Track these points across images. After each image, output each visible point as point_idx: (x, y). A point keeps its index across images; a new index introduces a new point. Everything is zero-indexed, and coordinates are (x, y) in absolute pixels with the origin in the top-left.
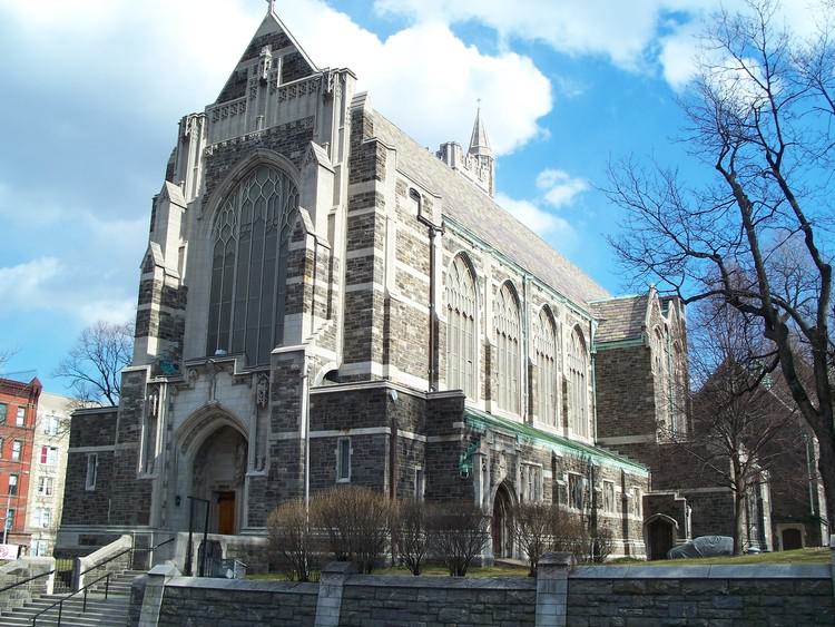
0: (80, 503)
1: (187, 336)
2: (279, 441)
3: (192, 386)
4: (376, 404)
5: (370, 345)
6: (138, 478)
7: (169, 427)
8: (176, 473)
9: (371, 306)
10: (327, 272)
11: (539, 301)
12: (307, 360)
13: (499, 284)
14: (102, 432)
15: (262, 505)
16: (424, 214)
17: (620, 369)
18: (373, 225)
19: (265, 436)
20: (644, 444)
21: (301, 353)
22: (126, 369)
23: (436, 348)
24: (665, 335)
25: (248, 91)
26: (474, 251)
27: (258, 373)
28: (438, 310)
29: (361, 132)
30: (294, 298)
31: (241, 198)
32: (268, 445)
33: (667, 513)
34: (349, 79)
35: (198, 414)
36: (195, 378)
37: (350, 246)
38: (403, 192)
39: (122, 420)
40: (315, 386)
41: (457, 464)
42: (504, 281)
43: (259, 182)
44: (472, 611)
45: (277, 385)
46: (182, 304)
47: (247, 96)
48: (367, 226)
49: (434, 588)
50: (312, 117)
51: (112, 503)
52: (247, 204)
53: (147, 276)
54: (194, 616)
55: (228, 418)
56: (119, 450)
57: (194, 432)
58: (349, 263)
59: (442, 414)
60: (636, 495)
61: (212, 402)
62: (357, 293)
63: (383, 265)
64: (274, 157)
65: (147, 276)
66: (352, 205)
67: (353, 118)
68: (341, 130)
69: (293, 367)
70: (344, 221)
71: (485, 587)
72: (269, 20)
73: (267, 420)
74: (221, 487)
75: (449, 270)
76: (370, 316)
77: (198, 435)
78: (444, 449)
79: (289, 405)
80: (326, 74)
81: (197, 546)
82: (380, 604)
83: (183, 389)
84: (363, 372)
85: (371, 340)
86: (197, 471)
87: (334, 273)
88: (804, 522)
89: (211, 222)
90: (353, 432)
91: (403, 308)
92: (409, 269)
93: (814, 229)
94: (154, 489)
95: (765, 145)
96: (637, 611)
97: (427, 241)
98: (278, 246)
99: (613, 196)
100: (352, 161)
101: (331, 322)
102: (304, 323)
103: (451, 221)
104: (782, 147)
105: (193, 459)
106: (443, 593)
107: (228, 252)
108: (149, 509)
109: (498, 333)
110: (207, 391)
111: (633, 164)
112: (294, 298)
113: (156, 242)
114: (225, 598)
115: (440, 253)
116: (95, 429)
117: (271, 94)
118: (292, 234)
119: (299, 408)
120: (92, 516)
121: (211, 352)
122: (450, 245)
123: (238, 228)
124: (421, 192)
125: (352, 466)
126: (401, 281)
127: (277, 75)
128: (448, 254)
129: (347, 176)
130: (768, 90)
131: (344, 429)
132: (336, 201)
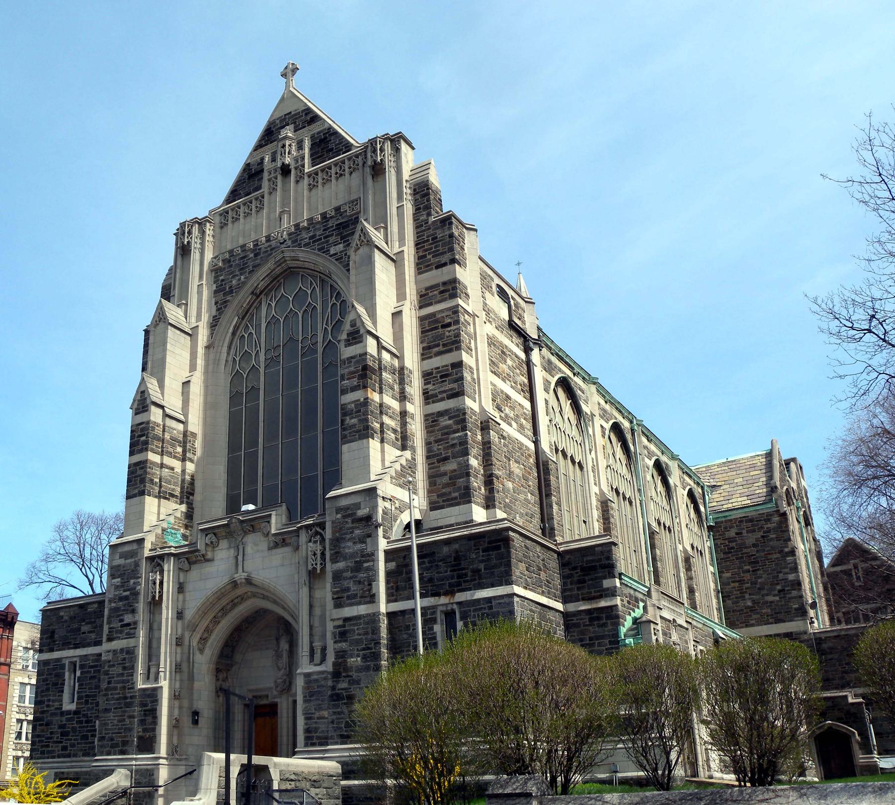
0: (55, 729)
2: (346, 620)
4: (493, 554)
5: (468, 481)
7: (180, 615)
8: (191, 678)
9: (464, 428)
10: (396, 387)
11: (650, 455)
12: (381, 504)
13: (607, 426)
14: (85, 628)
15: (325, 713)
18: (457, 322)
19: (323, 617)
21: (372, 492)
22: (114, 541)
23: (549, 495)
24: (795, 501)
25: (265, 185)
27: (308, 527)
28: (545, 446)
29: (428, 207)
30: (354, 421)
32: (330, 626)
34: (404, 147)
35: (220, 594)
36: (213, 545)
37: (426, 353)
38: (488, 288)
39: (111, 610)
40: (393, 538)
43: (288, 292)
45: (337, 541)
48: (449, 325)
51: (101, 725)
52: (272, 322)
53: (141, 418)
55: (265, 597)
57: (216, 621)
58: (427, 376)
59: (583, 569)
61: (240, 576)
62: (441, 414)
63: (475, 376)
64: (307, 256)
65: (141, 418)
66: (424, 300)
67: (415, 192)
68: (400, 208)
69: (362, 512)
70: (415, 322)
73: (326, 592)
74: (255, 697)
75: (551, 397)
76: (464, 442)
77: (220, 625)
79: (358, 567)
80: (372, 142)
81: (235, 771)
83: (195, 562)
84: (461, 519)
85: (468, 475)
86: (221, 676)
87: (408, 389)
89: (225, 349)
90: (461, 597)
92: (506, 387)
97: (522, 356)
100: (418, 245)
101: (408, 454)
102: (372, 453)
105: (215, 658)
107: (250, 386)
110: (232, 561)
112: (354, 421)
113: (152, 375)
115: (539, 375)
116: (75, 626)
118: (344, 336)
119: (374, 570)
120: (73, 746)
121: (233, 506)
122: (549, 367)
127: (303, 158)
128: (549, 378)
129: (413, 265)
131: (446, 594)
132: (401, 296)
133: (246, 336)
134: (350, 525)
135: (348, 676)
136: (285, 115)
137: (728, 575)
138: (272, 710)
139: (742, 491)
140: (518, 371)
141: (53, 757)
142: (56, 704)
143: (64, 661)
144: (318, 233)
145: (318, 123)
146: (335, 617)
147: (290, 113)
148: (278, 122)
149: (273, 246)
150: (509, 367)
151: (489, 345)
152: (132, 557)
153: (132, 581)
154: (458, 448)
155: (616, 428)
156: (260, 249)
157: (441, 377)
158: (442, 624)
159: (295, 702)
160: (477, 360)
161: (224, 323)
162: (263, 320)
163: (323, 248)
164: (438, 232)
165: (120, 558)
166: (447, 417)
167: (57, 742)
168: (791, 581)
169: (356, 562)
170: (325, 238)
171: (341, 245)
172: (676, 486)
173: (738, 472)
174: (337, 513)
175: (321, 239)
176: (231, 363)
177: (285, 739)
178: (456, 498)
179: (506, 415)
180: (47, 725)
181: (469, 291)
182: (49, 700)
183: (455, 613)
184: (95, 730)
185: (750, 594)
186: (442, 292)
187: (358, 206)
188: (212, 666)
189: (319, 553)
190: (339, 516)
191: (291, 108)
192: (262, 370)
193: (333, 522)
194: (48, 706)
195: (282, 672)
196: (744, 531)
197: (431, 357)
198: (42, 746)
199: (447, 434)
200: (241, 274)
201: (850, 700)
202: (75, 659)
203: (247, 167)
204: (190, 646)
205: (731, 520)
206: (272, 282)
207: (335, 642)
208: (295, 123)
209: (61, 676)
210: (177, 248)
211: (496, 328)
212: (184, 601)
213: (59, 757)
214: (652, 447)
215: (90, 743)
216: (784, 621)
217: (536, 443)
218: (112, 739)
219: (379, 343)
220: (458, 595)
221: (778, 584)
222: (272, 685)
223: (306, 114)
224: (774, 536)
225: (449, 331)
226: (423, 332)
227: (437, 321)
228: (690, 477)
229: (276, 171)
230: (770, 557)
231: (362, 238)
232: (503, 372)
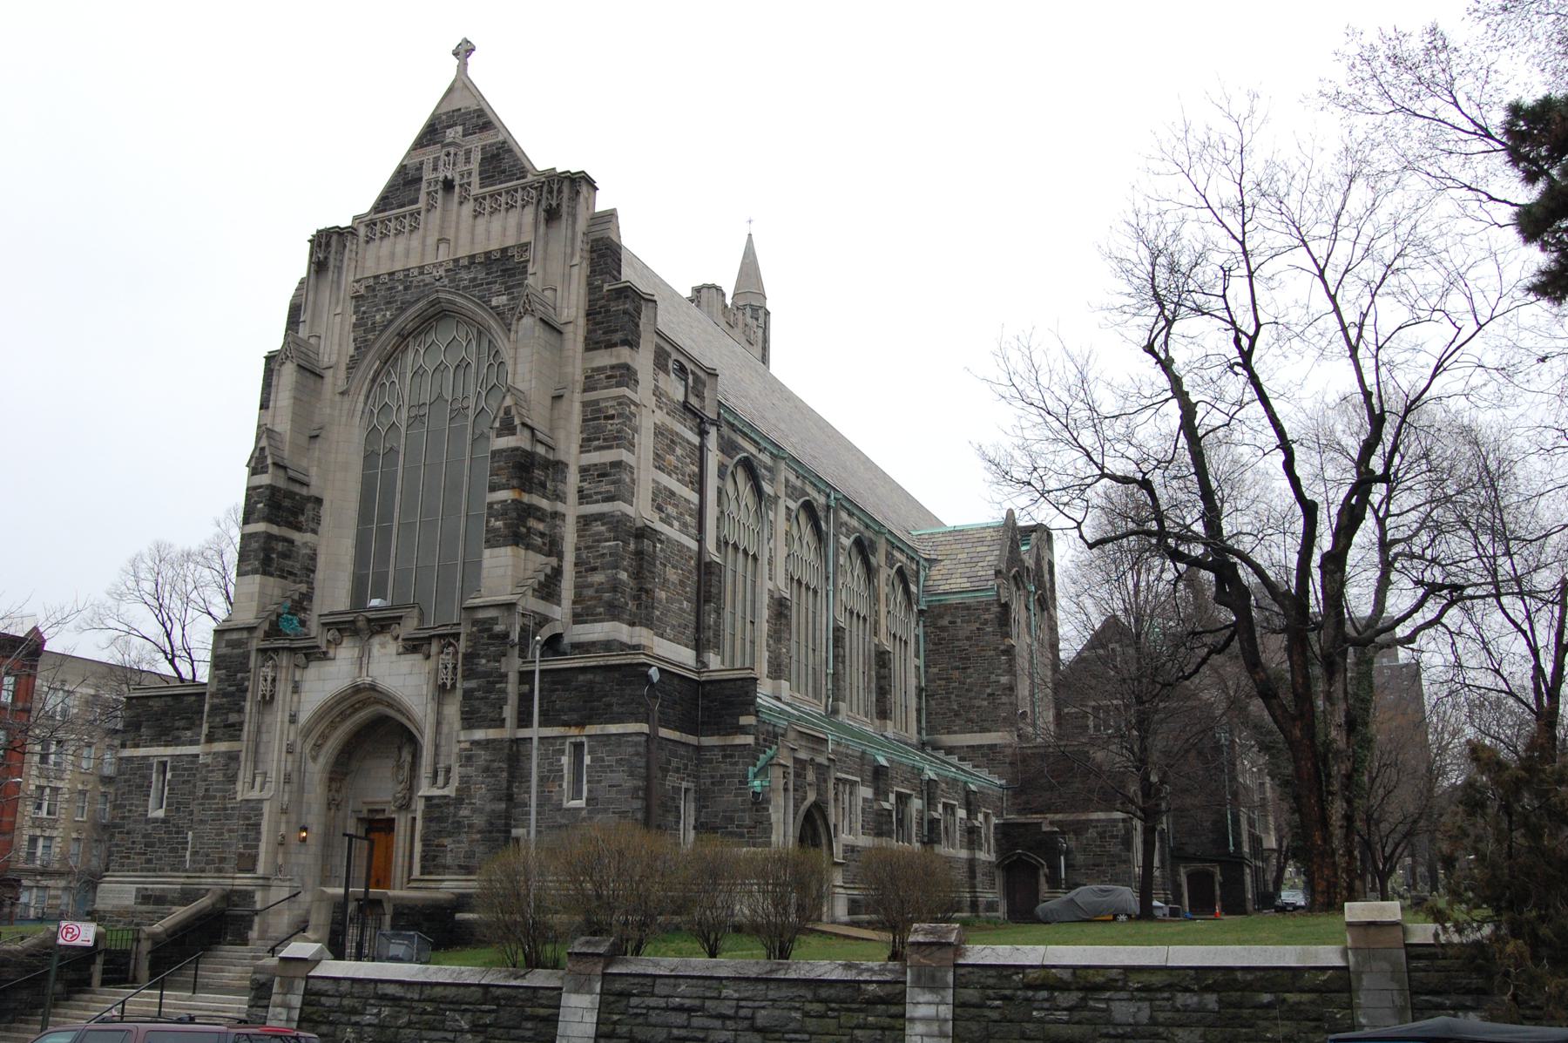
0: (139, 838)
1: (320, 575)
2: (474, 743)
3: (331, 653)
6: (239, 798)
16: (693, 401)
17: (962, 634)
25: (423, 197)
26: (761, 456)
31: (410, 362)
32: (456, 749)
33: (1030, 849)
35: (340, 699)
42: (801, 500)
44: (807, 1014)
45: (469, 657)
46: (312, 525)
47: (422, 204)
49: (748, 979)
50: (527, 244)
54: (357, 1024)
55: (390, 706)
57: (333, 726)
60: (987, 822)
69: (499, 628)
71: (825, 977)
73: (453, 710)
74: (370, 811)
78: (725, 756)
82: (662, 1003)
86: (334, 786)
88: (1219, 862)
89: (362, 398)
91: (661, 542)
94: (266, 816)
95: (1233, 323)
96: (1064, 1015)
98: (469, 442)
99: (1001, 389)
103: (727, 409)
104: (1258, 326)
106: (761, 987)
108: (257, 847)
114: (409, 996)
115: (713, 459)
117: (461, 203)
124: (689, 366)
125: (588, 782)
126: (660, 500)
128: (727, 461)
130: (1242, 243)
131: (577, 725)
134: (486, 641)
137: (935, 670)
138: (389, 825)
140: (688, 460)
141: (136, 870)
144: (480, 276)
145: (492, 132)
146: (462, 738)
148: (444, 117)
152: (240, 647)
154: (608, 558)
155: (808, 507)
157: (599, 476)
159: (414, 819)
163: (484, 296)
164: (612, 304)
169: (488, 682)
170: (488, 284)
171: (505, 297)
172: (879, 566)
174: (473, 625)
176: (367, 415)
177: (399, 874)
180: (128, 833)
181: (640, 376)
182: (131, 805)
186: (609, 377)
188: (326, 775)
189: (450, 666)
190: (475, 629)
191: (459, 102)
192: (403, 430)
197: (589, 451)
199: (598, 541)
201: (1046, 828)
203: (402, 169)
205: (946, 606)
208: (464, 124)
209: (147, 777)
210: (311, 262)
212: (299, 702)
214: (854, 523)
218: (208, 855)
219: (533, 434)
220: (588, 727)
222: (390, 799)
226: (584, 421)
227: (600, 410)
228: (902, 551)
229: (437, 182)
230: (983, 653)
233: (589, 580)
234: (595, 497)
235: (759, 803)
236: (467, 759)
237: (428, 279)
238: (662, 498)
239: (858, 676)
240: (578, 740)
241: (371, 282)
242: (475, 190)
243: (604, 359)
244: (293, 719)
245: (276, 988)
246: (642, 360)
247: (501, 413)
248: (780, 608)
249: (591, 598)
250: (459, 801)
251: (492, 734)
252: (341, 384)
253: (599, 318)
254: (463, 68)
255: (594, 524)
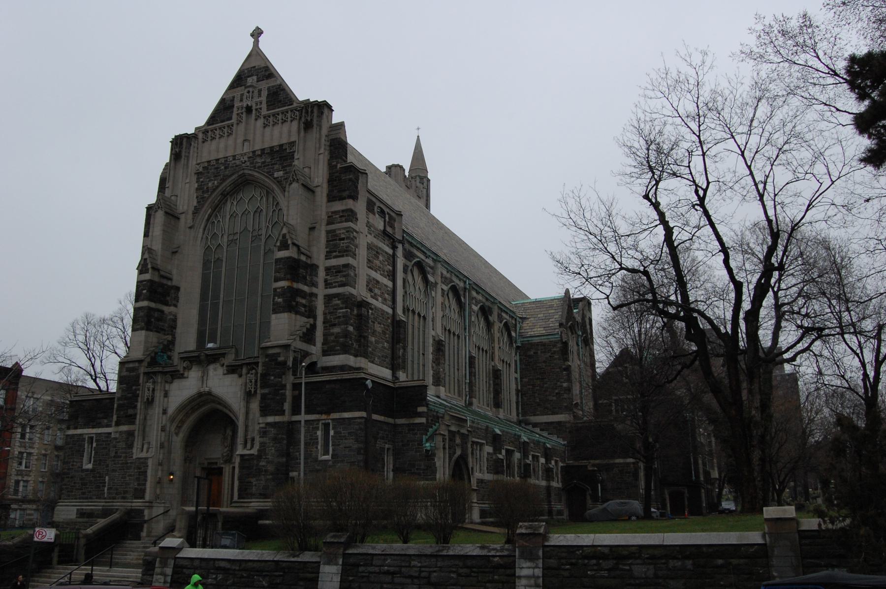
1: (179, 330)
2: (268, 424)
3: (186, 375)
8: (170, 452)
16: (389, 229)
20: (561, 422)
25: (234, 116)
26: (427, 260)
32: (257, 427)
36: (188, 369)
41: (420, 443)
44: (459, 575)
45: (264, 376)
46: (174, 302)
47: (234, 120)
51: (109, 480)
56: (116, 432)
57: (187, 415)
69: (281, 359)
72: (256, 53)
73: (255, 406)
74: (209, 464)
82: (377, 569)
89: (201, 230)
92: (377, 276)
93: (731, 253)
95: (694, 181)
98: (262, 252)
99: (563, 220)
103: (408, 234)
104: (708, 183)
107: (216, 257)
108: (145, 485)
109: (445, 329)
111: (582, 195)
117: (256, 119)
120: (90, 492)
123: (225, 237)
125: (332, 445)
126: (370, 286)
128: (408, 263)
130: (699, 137)
133: (216, 222)
135: (266, 458)
136: (251, 68)
138: (220, 471)
139: (541, 324)
141: (76, 499)
142: (79, 464)
143: (84, 436)
145: (273, 79)
146: (261, 422)
147: (255, 67)
148: (246, 71)
149: (238, 164)
150: (380, 261)
151: (368, 249)
153: (134, 388)
154: (342, 319)
155: (454, 289)
156: (229, 164)
158: (322, 431)
159: (234, 468)
160: (359, 262)
161: (202, 213)
162: (228, 214)
163: (270, 172)
165: (126, 371)
166: (336, 299)
167: (78, 489)
168: (565, 388)
171: (282, 172)
173: (542, 310)
174: (266, 358)
175: (269, 165)
178: (338, 350)
179: (375, 294)
180: (72, 477)
182: (74, 462)
183: (329, 425)
184: (105, 483)
185: (538, 394)
186: (341, 217)
187: (294, 148)
190: (267, 360)
193: (263, 363)
194: (73, 465)
195: (226, 449)
196: (539, 352)
197: (330, 259)
198: (68, 491)
199: (336, 309)
200: (215, 180)
201: (590, 468)
202: (92, 435)
203: (223, 101)
204: (170, 431)
205: (531, 344)
206: (235, 188)
207: (260, 437)
208: (257, 75)
211: (374, 237)
212: (168, 402)
213: (80, 499)
214: (480, 297)
215: (101, 491)
216: (557, 414)
217: (394, 309)
218: (117, 489)
221: (556, 389)
222: (220, 456)
223: (266, 71)
224: (557, 357)
225: (343, 243)
226: (327, 241)
227: (336, 235)
229: (242, 108)
230: (553, 370)
231: (294, 177)
232: (376, 265)
233: (331, 331)
234: (334, 285)
235: (430, 456)
236: (263, 433)
237: (238, 162)
238: (372, 285)
239: (483, 384)
240: (327, 421)
241: (206, 165)
242: (264, 112)
243: (338, 206)
244: (165, 412)
245: (157, 565)
246: (360, 207)
247: (281, 238)
248: (439, 346)
249: (333, 341)
250: (259, 457)
251: (278, 419)
252: (190, 222)
253: (335, 183)
254: (256, 43)
255: (334, 299)
